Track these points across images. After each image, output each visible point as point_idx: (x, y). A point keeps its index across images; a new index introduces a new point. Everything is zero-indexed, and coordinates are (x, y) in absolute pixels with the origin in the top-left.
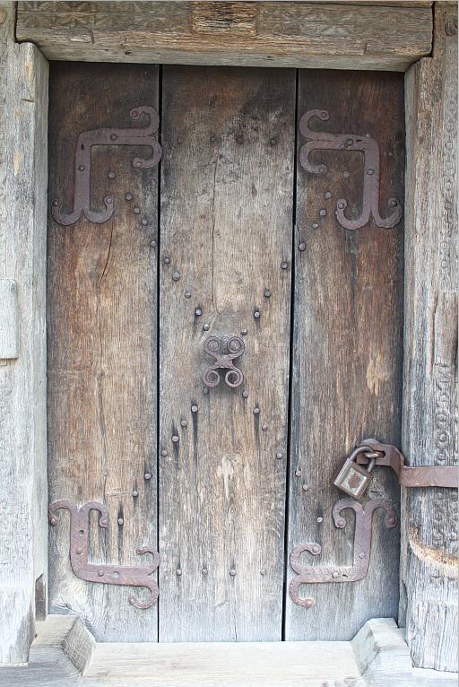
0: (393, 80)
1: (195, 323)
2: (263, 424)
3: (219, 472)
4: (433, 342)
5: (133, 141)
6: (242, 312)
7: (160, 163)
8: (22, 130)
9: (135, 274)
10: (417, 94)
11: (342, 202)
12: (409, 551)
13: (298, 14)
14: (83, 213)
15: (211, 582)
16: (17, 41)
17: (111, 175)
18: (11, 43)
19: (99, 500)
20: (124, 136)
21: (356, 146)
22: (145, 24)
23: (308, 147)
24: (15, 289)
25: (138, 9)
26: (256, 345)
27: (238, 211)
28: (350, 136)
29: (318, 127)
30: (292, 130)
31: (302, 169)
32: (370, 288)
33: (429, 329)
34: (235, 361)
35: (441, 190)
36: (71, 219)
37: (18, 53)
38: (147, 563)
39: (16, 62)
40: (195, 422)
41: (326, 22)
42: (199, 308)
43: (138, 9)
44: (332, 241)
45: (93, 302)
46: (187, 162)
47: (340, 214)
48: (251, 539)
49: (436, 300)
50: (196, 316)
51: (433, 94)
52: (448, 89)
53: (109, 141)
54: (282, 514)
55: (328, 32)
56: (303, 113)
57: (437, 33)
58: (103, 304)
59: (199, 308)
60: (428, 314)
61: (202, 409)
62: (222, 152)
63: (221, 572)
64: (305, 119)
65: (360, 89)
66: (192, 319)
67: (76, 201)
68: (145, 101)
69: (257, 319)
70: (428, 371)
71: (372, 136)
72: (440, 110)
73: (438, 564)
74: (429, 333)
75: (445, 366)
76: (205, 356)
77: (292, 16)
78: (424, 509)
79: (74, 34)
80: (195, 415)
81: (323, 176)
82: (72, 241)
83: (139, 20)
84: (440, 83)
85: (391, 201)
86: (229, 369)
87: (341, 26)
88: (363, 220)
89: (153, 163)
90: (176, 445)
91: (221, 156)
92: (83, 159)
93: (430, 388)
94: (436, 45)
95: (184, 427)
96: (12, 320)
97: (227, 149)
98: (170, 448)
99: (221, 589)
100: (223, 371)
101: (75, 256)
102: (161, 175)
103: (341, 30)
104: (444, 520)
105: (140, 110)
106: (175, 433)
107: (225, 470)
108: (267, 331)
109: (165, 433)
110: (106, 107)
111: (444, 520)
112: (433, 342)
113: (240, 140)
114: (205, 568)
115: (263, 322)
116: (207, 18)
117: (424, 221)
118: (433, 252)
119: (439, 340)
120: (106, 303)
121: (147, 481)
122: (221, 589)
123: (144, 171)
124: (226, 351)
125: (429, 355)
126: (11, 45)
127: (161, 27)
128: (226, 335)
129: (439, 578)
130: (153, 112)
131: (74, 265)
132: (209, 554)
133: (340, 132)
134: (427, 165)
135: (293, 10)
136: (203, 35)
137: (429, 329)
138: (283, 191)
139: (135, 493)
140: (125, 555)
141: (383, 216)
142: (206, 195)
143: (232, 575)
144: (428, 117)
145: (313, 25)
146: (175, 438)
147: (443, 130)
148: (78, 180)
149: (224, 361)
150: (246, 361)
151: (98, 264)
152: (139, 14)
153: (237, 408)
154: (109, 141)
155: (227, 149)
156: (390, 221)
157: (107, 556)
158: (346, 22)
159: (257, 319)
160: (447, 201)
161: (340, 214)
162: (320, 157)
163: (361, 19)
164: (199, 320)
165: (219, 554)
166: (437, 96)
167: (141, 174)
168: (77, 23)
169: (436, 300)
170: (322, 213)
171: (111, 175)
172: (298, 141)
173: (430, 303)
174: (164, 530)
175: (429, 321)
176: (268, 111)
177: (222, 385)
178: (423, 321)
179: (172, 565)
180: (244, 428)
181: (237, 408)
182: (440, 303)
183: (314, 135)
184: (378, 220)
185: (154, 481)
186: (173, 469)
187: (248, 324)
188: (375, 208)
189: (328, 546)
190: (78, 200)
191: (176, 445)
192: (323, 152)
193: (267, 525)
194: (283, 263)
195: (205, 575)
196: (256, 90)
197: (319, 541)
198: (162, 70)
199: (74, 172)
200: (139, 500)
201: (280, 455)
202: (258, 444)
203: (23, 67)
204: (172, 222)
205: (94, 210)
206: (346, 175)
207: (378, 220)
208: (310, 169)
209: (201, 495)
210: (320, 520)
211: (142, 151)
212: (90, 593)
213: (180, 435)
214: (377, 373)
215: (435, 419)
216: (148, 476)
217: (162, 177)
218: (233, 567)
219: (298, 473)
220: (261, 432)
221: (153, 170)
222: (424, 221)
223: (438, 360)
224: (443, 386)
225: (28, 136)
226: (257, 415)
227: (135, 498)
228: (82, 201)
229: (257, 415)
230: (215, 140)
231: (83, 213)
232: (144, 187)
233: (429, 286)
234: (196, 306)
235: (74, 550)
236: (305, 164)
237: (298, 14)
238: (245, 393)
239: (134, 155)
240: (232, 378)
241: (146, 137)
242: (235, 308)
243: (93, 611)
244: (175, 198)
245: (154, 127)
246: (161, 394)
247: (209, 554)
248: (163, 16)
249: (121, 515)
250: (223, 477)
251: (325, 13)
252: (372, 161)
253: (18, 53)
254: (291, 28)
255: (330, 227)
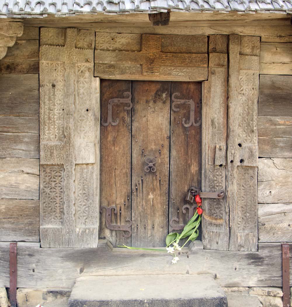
0: (200, 83)
1: (142, 154)
2: (162, 183)
3: (149, 197)
4: (208, 158)
5: (124, 102)
6: (156, 151)
7: (132, 109)
8: (96, 101)
9: (124, 141)
10: (205, 85)
11: (184, 119)
12: (203, 217)
13: (171, 69)
14: (110, 123)
15: (147, 230)
16: (94, 77)
17: (118, 112)
18: (93, 77)
19: (114, 206)
20: (122, 100)
21: (188, 103)
22: (129, 72)
23: (174, 104)
24: (95, 145)
25: (127, 68)
26: (160, 160)
27: (155, 120)
28: (186, 100)
29: (177, 97)
30: (169, 99)
31: (172, 110)
32: (192, 144)
33: (207, 155)
34: (154, 165)
35: (210, 117)
36: (106, 124)
37: (95, 80)
38: (128, 225)
39: (94, 83)
40: (142, 182)
41: (178, 71)
42: (143, 150)
43: (127, 68)
44: (181, 130)
45: (113, 148)
46: (139, 107)
47: (183, 122)
48: (159, 219)
49: (209, 147)
50: (143, 152)
51: (208, 91)
52: (212, 89)
53: (117, 102)
54: (167, 209)
55: (179, 74)
56: (173, 94)
57: (209, 74)
58: (116, 149)
59: (143, 150)
60: (207, 151)
61: (144, 178)
62: (150, 105)
63: (150, 227)
64: (173, 96)
65: (189, 86)
66: (141, 153)
67: (108, 119)
68: (127, 90)
69: (160, 153)
70: (207, 166)
71: (193, 100)
72: (210, 95)
73: (211, 220)
74: (207, 156)
75: (211, 165)
76: (144, 164)
77: (169, 70)
78: (206, 205)
79: (110, 75)
80: (142, 180)
81: (178, 112)
82: (107, 131)
83: (127, 71)
84: (210, 88)
85: (198, 119)
86: (152, 167)
87: (183, 72)
88: (190, 124)
89: (130, 108)
90: (137, 189)
91: (149, 106)
92: (110, 107)
93: (208, 171)
94: (209, 77)
95: (139, 184)
96: (94, 153)
97: (151, 104)
98: (135, 190)
99: (149, 233)
100: (150, 167)
101: (108, 135)
102: (132, 112)
103: (183, 74)
104: (212, 208)
105: (126, 93)
106: (136, 186)
107: (151, 196)
108: (162, 156)
109: (133, 187)
110: (116, 92)
111: (212, 208)
112: (208, 158)
113: (155, 102)
114: (145, 225)
115: (162, 154)
116: (147, 72)
117: (206, 125)
118: (208, 134)
119: (209, 158)
120: (117, 149)
121: (128, 200)
122: (149, 233)
123: (128, 111)
124: (151, 162)
125: (207, 162)
126: (93, 78)
127: (134, 73)
128: (152, 158)
129: (211, 224)
130: (130, 93)
131: (107, 139)
132: (146, 221)
133: (184, 99)
134: (206, 110)
135: (169, 68)
136: (145, 76)
137: (207, 155)
138: (167, 116)
139: (125, 203)
140: (122, 222)
141: (196, 123)
142: (145, 118)
143: (153, 228)
144: (207, 97)
145: (175, 73)
146: (136, 187)
147: (211, 101)
148: (109, 113)
149: (151, 164)
150: (156, 165)
151: (114, 138)
152: (127, 69)
153: (154, 178)
154: (117, 102)
155: (151, 104)
156: (198, 125)
157: (116, 222)
158: (184, 72)
159: (160, 153)
160: (212, 120)
161: (183, 122)
162: (178, 106)
163: (188, 71)
164: (143, 153)
165: (149, 221)
166: (209, 91)
167: (126, 111)
168: (111, 72)
169: (209, 147)
170: (178, 122)
171: (118, 112)
172: (171, 102)
173: (207, 148)
174: (133, 214)
175: (207, 153)
176: (163, 93)
177: (150, 171)
178: (206, 153)
179: (136, 225)
180: (156, 183)
181: (154, 178)
182: (210, 148)
183: (176, 100)
184: (194, 124)
185: (130, 200)
186: (136, 196)
187: (157, 155)
188: (193, 121)
189: (181, 220)
190: (108, 119)
191: (137, 189)
192: (178, 105)
193: (163, 213)
194: (167, 137)
195: (145, 228)
196: (159, 87)
197: (178, 217)
198: (132, 82)
199: (107, 111)
200: (126, 206)
201: (167, 192)
202: (160, 188)
203: (97, 83)
204: (135, 125)
205: (113, 122)
206: (185, 111)
207: (194, 124)
208: (175, 110)
209: (144, 204)
210: (178, 211)
211: (127, 105)
212: (111, 233)
213: (138, 186)
214: (194, 169)
215: (209, 180)
216: (128, 198)
217: (133, 112)
218: (153, 225)
219: (172, 197)
220: (161, 185)
221: (130, 110)
222: (206, 125)
223: (210, 163)
224: (211, 171)
225: (97, 103)
226: (160, 180)
227: (125, 205)
228: (110, 119)
229: (160, 180)
230: (147, 102)
231: (110, 123)
232: (127, 115)
233: (207, 143)
234: (143, 148)
235: (106, 220)
236: (173, 108)
237: (171, 69)
238: (157, 174)
239: (124, 106)
240: (153, 169)
241: (128, 101)
242: (154, 150)
243: (112, 239)
244: (136, 118)
245: (130, 98)
246: (132, 174)
247: (146, 221)
248: (134, 70)
249: (120, 210)
250: (150, 198)
251: (178, 69)
252: (193, 106)
253: (95, 80)
254: (169, 73)
255: (180, 125)
